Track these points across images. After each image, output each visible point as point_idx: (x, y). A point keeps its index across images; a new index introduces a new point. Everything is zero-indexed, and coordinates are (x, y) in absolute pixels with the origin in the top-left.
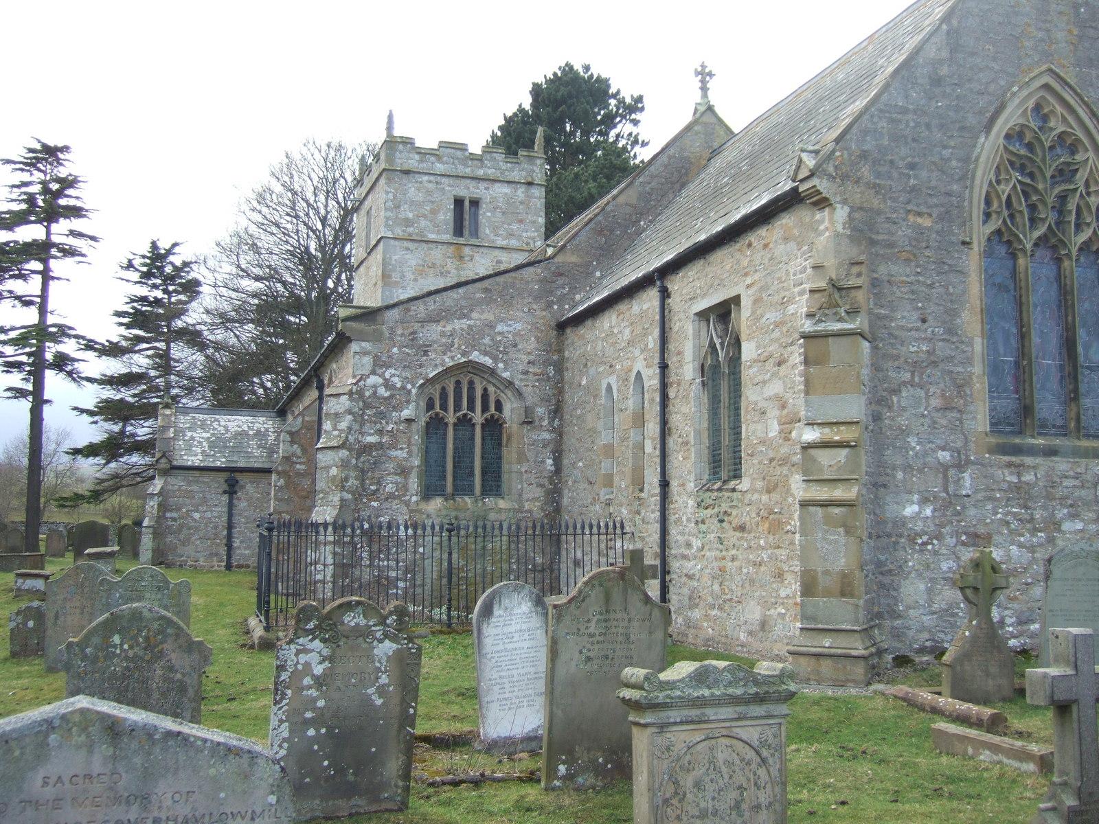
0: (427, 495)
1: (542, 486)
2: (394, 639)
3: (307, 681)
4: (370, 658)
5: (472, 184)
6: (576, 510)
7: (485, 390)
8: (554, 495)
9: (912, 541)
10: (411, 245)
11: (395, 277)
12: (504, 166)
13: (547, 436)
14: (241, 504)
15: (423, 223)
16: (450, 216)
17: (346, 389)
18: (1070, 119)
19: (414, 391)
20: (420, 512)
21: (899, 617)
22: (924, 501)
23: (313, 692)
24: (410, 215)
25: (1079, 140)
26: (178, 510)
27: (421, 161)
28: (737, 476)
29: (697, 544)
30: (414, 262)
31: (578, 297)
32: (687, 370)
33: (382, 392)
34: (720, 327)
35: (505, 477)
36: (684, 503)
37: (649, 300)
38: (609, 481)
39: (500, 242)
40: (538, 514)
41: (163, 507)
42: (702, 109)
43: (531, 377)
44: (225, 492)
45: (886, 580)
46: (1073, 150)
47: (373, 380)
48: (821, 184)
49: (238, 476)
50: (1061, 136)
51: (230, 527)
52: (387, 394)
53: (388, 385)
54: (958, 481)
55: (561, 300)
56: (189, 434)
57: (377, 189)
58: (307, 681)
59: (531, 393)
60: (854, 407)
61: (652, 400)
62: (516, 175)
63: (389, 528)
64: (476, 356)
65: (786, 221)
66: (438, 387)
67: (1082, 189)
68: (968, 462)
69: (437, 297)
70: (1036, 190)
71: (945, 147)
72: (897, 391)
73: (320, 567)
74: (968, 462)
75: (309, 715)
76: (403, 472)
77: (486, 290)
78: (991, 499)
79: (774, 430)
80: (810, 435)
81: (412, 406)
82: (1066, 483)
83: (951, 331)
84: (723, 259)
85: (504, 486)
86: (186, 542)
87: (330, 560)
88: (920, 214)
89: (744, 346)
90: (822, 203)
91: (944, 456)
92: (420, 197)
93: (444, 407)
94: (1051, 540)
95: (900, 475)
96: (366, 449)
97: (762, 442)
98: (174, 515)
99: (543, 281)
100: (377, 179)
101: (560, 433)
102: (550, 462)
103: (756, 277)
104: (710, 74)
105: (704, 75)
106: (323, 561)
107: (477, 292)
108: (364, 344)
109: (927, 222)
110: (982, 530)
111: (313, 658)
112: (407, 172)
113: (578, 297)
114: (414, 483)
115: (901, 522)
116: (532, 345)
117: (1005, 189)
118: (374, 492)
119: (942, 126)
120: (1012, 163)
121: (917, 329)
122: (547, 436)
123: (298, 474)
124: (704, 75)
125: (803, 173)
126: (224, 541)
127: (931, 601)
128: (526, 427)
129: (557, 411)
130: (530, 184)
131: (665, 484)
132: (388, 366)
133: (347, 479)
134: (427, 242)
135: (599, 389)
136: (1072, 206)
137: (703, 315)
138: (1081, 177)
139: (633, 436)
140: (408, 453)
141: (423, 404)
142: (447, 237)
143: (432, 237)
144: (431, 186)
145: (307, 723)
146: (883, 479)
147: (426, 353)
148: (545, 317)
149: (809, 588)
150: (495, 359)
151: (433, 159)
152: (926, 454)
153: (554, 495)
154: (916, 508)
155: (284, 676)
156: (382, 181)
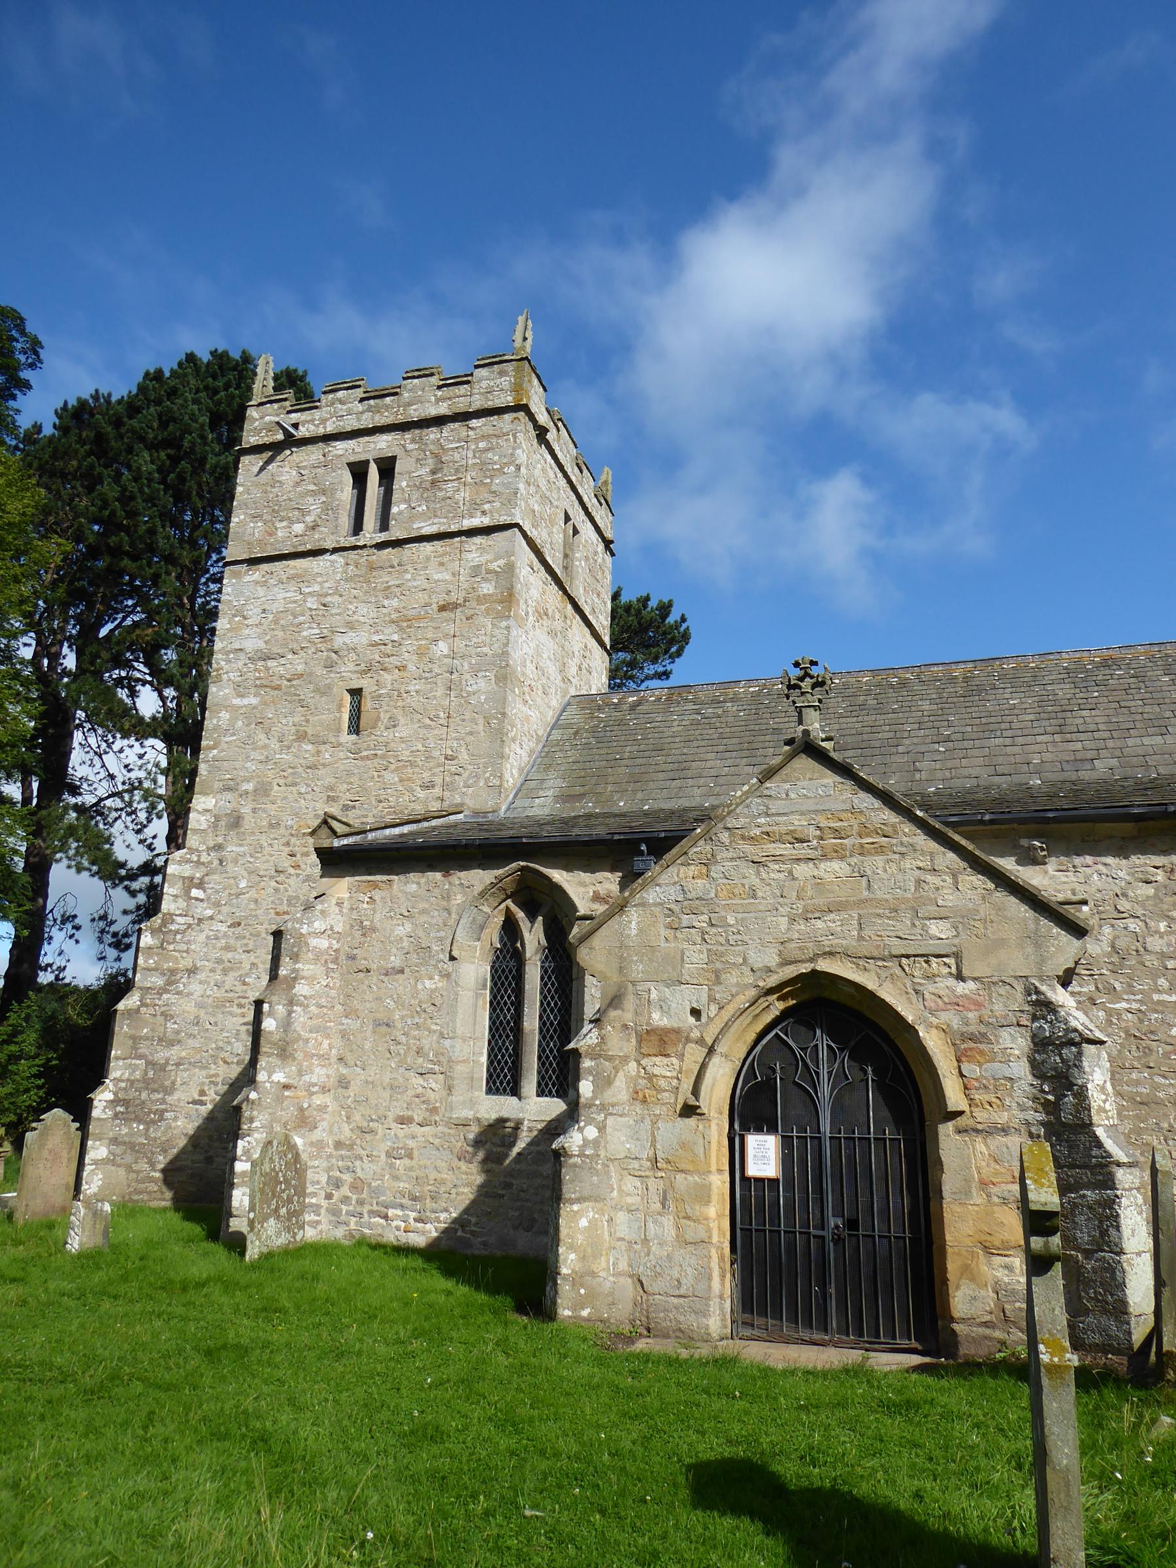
144: (552, 475)
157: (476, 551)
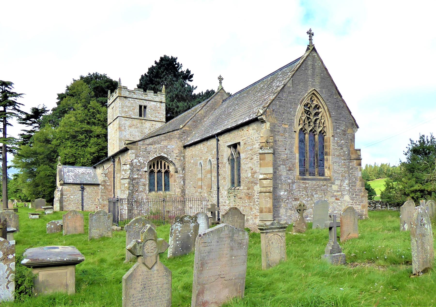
0: (150, 190)
1: (180, 188)
2: (194, 223)
3: (177, 232)
4: (189, 226)
5: (145, 101)
6: (190, 194)
7: (165, 163)
8: (183, 191)
9: (282, 200)
10: (127, 119)
11: (123, 128)
12: (154, 96)
13: (181, 175)
14: (85, 193)
15: (130, 113)
16: (138, 111)
17: (129, 163)
18: (318, 101)
19: (147, 163)
21: (280, 217)
22: (285, 191)
23: (178, 234)
25: (320, 106)
26: (66, 195)
27: (129, 94)
28: (239, 186)
29: (227, 202)
30: (128, 124)
31: (189, 139)
32: (224, 159)
33: (138, 164)
34: (234, 149)
35: (170, 186)
36: (224, 192)
37: (213, 142)
38: (201, 187)
39: (154, 119)
40: (179, 195)
41: (62, 195)
42: (220, 88)
43: (177, 160)
45: (277, 209)
46: (318, 109)
47: (135, 161)
48: (264, 117)
49: (85, 187)
50: (316, 105)
51: (83, 199)
54: (292, 186)
56: (68, 174)
57: (116, 101)
58: (177, 232)
59: (177, 165)
60: (270, 170)
61: (214, 167)
62: (157, 99)
63: (142, 199)
64: (162, 154)
65: (254, 126)
66: (153, 163)
67: (320, 118)
68: (295, 182)
69: (152, 139)
70: (310, 118)
71: (291, 108)
72: (279, 166)
73: (124, 210)
74: (295, 182)
75: (177, 239)
76: (144, 185)
77: (165, 137)
78: (299, 190)
79: (250, 175)
80: (261, 177)
81: (146, 168)
82: (315, 186)
83: (291, 152)
84: (236, 133)
85: (170, 189)
87: (126, 208)
88: (285, 124)
89: (241, 154)
90: (263, 122)
91: (290, 181)
92: (129, 105)
93: (154, 167)
94: (312, 199)
95: (280, 185)
96: (134, 179)
97: (246, 178)
99: (180, 134)
100: (116, 99)
101: (184, 174)
102: (182, 182)
103: (245, 138)
104: (222, 79)
106: (124, 209)
107: (162, 137)
109: (287, 126)
110: (297, 197)
111: (178, 227)
112: (125, 97)
113: (189, 139)
114: (147, 188)
115: (280, 196)
116: (177, 151)
117: (303, 118)
118: (137, 191)
119: (290, 103)
120: (305, 112)
121: (284, 152)
122: (181, 175)
123: (108, 185)
124: (221, 79)
125: (259, 114)
127: (286, 214)
128: (176, 173)
129: (184, 169)
130: (161, 102)
131: (218, 188)
132: (139, 157)
133: (130, 187)
134: (132, 118)
135: (197, 163)
136: (318, 122)
137: (229, 146)
138: (320, 115)
139: (209, 176)
140: (145, 180)
141: (149, 167)
142: (138, 117)
143: (133, 117)
144: (132, 101)
145: (177, 240)
146: (276, 187)
147: (149, 153)
148: (181, 144)
149: (261, 212)
150: (168, 155)
151: (133, 93)
152: (285, 180)
153: (183, 191)
154: (283, 193)
155: (173, 231)
156: (118, 99)
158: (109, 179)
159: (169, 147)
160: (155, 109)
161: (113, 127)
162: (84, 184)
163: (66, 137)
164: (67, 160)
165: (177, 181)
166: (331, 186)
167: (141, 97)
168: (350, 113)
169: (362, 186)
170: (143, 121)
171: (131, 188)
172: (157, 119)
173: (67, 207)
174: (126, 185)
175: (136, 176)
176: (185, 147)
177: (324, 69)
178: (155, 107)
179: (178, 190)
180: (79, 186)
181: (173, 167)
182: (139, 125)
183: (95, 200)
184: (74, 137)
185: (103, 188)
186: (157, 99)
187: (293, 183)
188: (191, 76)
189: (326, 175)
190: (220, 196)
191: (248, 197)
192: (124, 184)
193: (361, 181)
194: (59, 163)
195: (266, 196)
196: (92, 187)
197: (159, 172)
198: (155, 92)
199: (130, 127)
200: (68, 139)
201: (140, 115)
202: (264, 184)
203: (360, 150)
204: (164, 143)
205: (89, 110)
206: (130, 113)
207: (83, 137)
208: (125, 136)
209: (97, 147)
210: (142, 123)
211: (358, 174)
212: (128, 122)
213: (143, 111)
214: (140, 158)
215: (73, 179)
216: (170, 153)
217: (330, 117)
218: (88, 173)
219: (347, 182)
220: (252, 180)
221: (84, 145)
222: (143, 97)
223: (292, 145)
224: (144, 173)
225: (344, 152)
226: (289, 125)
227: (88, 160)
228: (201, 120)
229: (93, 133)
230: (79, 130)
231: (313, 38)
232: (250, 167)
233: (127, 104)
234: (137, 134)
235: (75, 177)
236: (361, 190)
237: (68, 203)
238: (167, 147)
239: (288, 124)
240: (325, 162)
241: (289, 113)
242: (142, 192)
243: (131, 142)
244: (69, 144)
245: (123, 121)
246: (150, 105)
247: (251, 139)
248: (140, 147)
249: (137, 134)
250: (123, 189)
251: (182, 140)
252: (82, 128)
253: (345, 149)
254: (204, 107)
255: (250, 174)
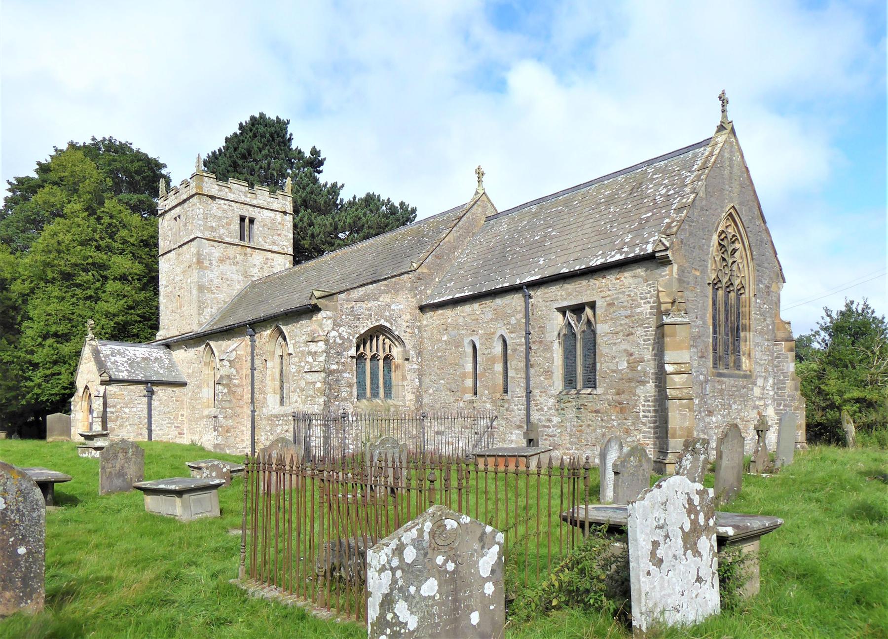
0: (359, 397)
5: (251, 208)
11: (206, 263)
13: (415, 366)
14: (155, 403)
15: (222, 231)
20: (358, 407)
24: (214, 224)
26: (114, 406)
30: (217, 255)
33: (338, 341)
35: (393, 388)
39: (267, 247)
40: (413, 408)
42: (481, 192)
43: (407, 334)
44: (145, 396)
49: (155, 388)
52: (341, 342)
53: (341, 338)
55: (421, 292)
56: (113, 359)
62: (275, 206)
64: (383, 322)
76: (350, 386)
77: (386, 285)
78: (714, 396)
86: (121, 426)
92: (219, 213)
96: (331, 372)
98: (113, 410)
99: (412, 282)
102: (417, 380)
105: (480, 174)
108: (328, 313)
109: (698, 273)
112: (213, 198)
116: (407, 317)
118: (336, 397)
122: (415, 366)
123: (235, 386)
124: (480, 174)
126: (146, 426)
130: (285, 213)
131: (529, 392)
132: (341, 326)
134: (225, 243)
137: (563, 311)
140: (350, 376)
143: (227, 240)
144: (226, 207)
148: (414, 303)
150: (391, 324)
151: (226, 190)
156: (194, 200)
157: (193, 247)
158: (238, 372)
159: (393, 307)
160: (272, 227)
161: (177, 259)
162: (154, 383)
163: (50, 275)
164: (53, 329)
165: (408, 377)
166: (752, 390)
167: (243, 199)
168: (776, 254)
169: (796, 390)
170: (248, 249)
171: (327, 391)
172: (275, 248)
173: (116, 433)
174: (319, 385)
175: (334, 367)
176: (422, 309)
177: (744, 169)
178: (273, 221)
179: (410, 397)
180: (142, 387)
181: (400, 349)
182: (239, 258)
183: (176, 418)
184: (67, 277)
185: (226, 390)
186: (276, 205)
187: (707, 381)
188: (321, 163)
189: (744, 367)
190: (533, 407)
191: (618, 409)
192: (314, 383)
193: (793, 380)
194: (91, 335)
195: (681, 405)
196: (169, 389)
197: (374, 358)
198: (272, 192)
199: (222, 261)
200: (52, 281)
201: (242, 238)
202: (675, 383)
203: (789, 323)
204: (385, 299)
205: (99, 219)
206: (222, 231)
207: (89, 277)
208: (212, 281)
209: (122, 302)
210: (246, 254)
211: (788, 367)
212: (217, 251)
213: (247, 228)
214: (342, 329)
215: (127, 370)
216: (396, 321)
217: (752, 259)
218: (156, 359)
219: (771, 381)
220: (630, 376)
221: (90, 297)
222: (248, 200)
223: (705, 308)
224: (350, 359)
225: (768, 325)
226: (701, 272)
227: (103, 329)
228: (449, 255)
229: (111, 270)
230: (79, 262)
231: (728, 107)
232: (626, 351)
233: (214, 211)
234: (235, 277)
235: (130, 365)
236: (793, 396)
237: (118, 423)
238: (390, 306)
239: (700, 268)
240: (742, 344)
241: (701, 248)
242: (347, 399)
243: (326, 294)
244: (55, 291)
245: (207, 248)
246: (262, 216)
247: (629, 296)
248: (342, 305)
249: (235, 277)
250: (311, 393)
251: (416, 295)
252: (86, 258)
253: (769, 321)
254: (455, 229)
255: (626, 364)
